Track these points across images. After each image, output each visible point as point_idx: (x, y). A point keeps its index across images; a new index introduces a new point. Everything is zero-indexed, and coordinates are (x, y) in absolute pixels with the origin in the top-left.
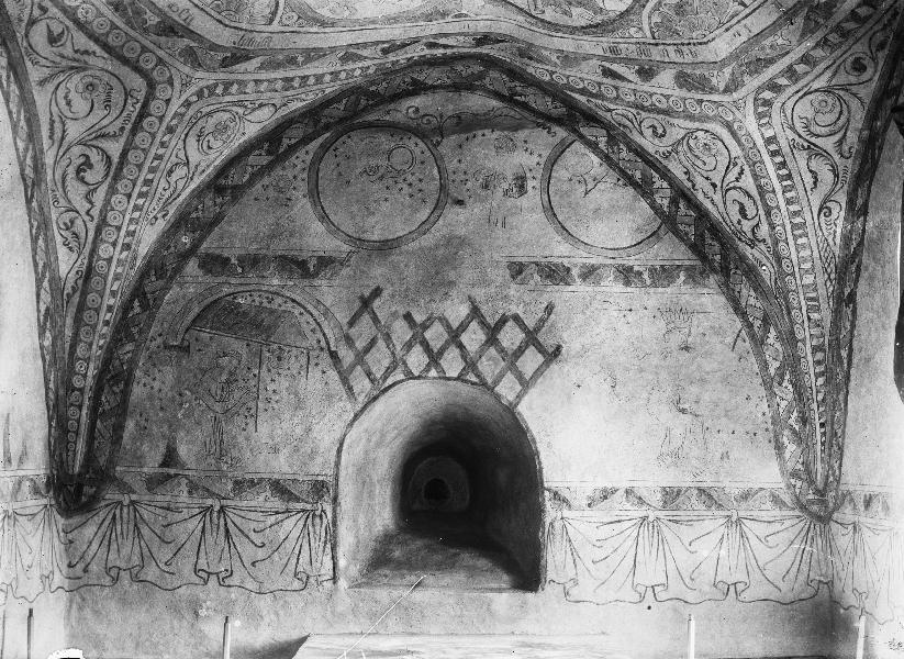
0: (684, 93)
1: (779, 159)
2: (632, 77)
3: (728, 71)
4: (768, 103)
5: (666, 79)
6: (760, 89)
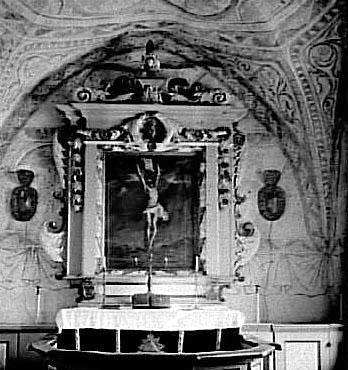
0: (257, 48)
1: (303, 78)
2: (235, 41)
3: (277, 36)
4: (297, 51)
5: (248, 41)
6: (293, 44)
